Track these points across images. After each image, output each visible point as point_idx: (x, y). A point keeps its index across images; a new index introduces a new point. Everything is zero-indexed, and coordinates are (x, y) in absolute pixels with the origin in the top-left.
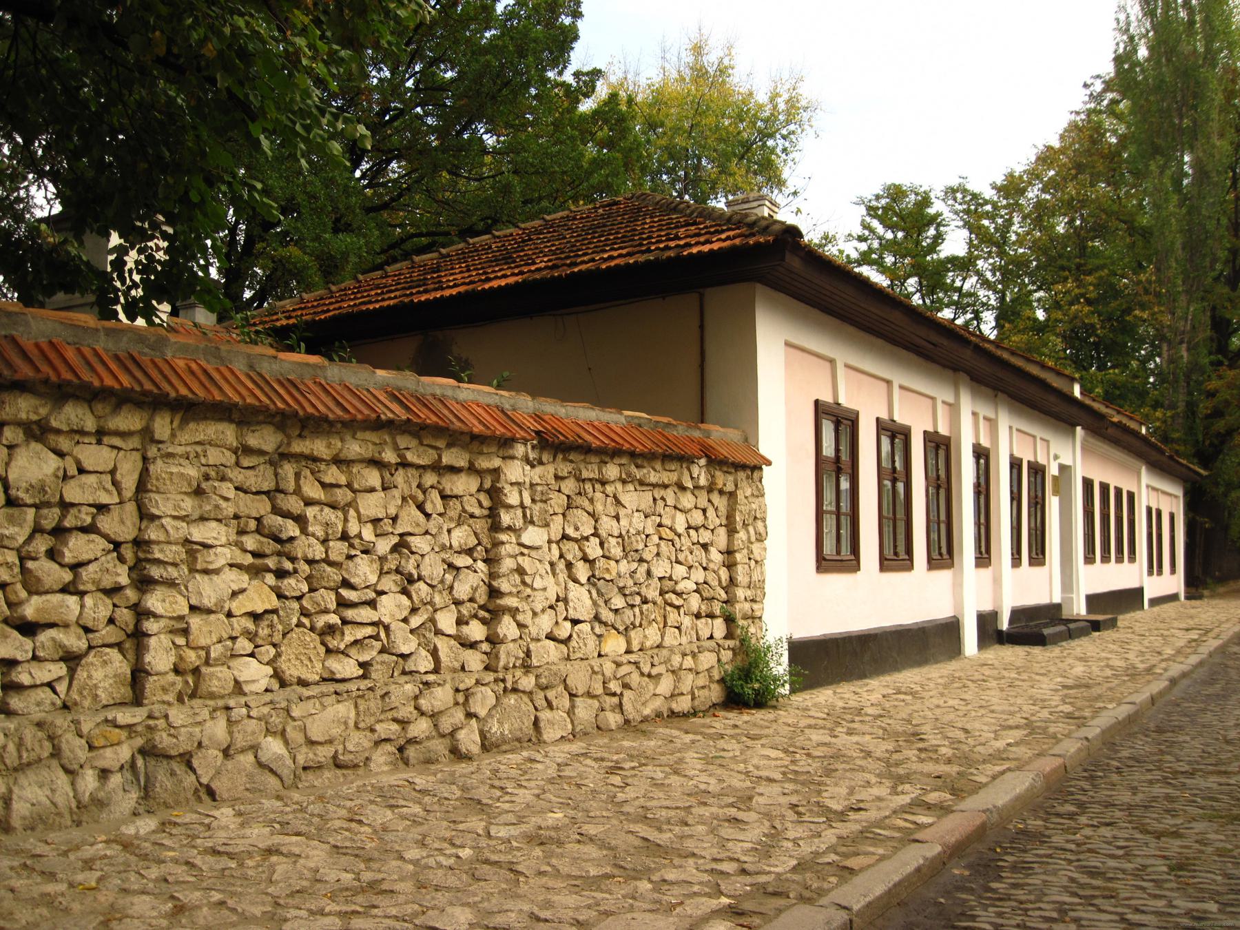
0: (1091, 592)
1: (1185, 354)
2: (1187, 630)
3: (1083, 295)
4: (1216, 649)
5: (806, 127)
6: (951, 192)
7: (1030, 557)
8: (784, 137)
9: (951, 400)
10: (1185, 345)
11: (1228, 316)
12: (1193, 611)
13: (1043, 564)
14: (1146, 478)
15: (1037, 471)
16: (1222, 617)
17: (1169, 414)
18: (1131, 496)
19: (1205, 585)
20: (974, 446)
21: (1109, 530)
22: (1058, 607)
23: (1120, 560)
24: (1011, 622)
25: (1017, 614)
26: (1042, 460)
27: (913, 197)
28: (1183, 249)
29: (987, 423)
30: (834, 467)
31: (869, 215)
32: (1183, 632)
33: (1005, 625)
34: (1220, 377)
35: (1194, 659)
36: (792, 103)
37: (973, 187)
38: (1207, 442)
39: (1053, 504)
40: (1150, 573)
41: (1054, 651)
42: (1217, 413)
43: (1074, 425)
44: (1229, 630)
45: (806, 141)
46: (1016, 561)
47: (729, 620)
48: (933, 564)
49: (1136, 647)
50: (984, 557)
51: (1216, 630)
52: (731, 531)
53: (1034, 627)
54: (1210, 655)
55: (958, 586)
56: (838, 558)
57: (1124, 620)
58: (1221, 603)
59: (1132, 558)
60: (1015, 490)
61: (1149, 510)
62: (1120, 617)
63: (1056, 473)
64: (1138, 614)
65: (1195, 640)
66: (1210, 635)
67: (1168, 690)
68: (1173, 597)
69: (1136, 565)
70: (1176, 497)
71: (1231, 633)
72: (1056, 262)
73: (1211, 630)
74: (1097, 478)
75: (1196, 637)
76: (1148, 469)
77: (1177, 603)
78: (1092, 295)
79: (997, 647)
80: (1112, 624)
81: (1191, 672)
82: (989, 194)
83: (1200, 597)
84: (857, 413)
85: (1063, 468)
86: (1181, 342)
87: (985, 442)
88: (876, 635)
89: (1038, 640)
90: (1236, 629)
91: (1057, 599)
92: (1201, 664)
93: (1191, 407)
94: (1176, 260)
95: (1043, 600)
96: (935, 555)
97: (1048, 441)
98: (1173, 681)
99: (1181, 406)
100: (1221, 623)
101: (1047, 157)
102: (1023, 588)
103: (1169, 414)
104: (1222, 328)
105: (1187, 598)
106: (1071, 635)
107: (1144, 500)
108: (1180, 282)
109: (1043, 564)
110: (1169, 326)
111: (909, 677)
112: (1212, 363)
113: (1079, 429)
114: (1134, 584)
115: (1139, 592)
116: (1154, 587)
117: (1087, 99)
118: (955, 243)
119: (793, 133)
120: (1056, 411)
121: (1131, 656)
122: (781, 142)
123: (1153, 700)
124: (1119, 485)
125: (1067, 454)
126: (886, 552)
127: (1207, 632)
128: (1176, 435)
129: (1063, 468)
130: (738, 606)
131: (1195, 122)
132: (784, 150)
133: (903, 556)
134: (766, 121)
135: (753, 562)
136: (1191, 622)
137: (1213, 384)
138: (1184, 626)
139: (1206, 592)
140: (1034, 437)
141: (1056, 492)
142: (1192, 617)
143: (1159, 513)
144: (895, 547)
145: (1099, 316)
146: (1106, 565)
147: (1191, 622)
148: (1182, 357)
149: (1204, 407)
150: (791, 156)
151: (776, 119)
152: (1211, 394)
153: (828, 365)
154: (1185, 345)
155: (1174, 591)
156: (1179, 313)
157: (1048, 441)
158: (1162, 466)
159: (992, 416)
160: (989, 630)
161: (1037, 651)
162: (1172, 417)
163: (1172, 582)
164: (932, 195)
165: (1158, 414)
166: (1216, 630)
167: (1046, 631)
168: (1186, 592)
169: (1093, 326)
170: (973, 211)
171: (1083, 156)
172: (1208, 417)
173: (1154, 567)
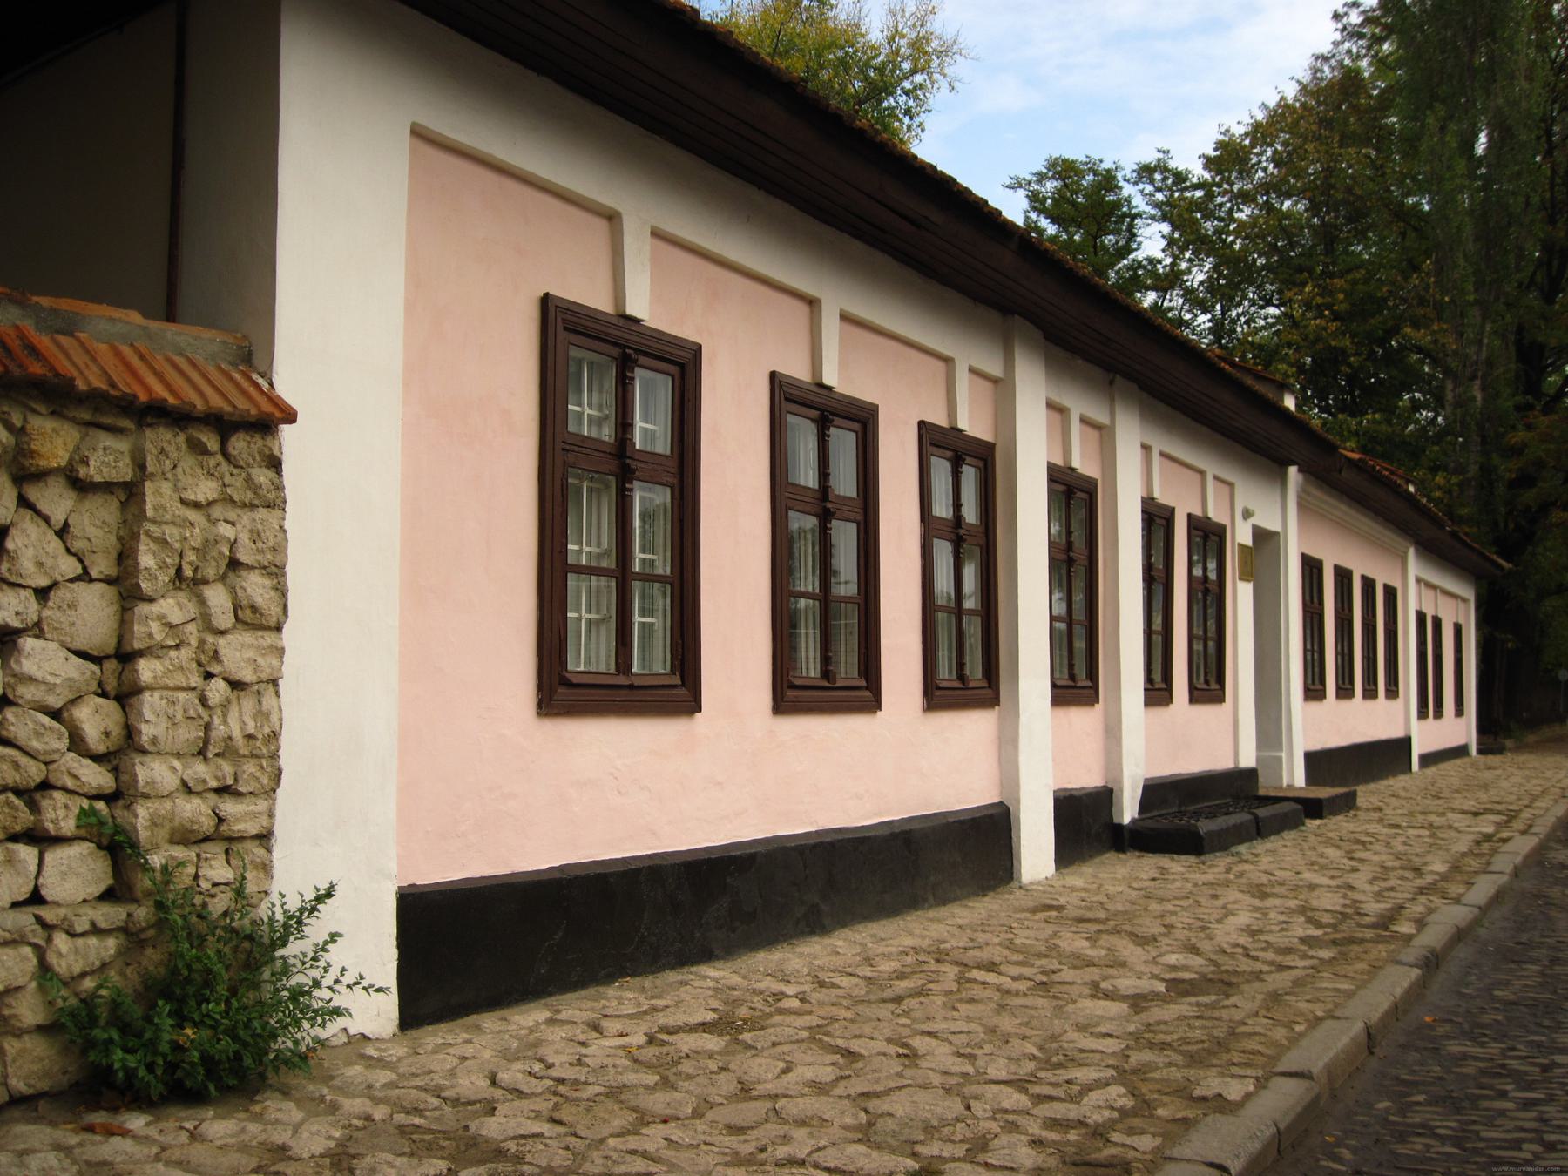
0: (1317, 745)
1: (1479, 396)
2: (1476, 814)
3: (1329, 307)
4: (1527, 857)
5: (936, 76)
6: (1145, 172)
7: (1192, 688)
8: (907, 93)
9: (995, 368)
10: (1478, 382)
11: (1540, 339)
12: (1488, 775)
13: (1219, 699)
14: (1415, 567)
15: (1208, 536)
16: (1535, 786)
17: (1454, 480)
18: (1390, 593)
19: (1508, 733)
20: (1052, 468)
21: (1348, 644)
22: (1251, 774)
23: (1370, 693)
24: (1144, 806)
25: (1155, 792)
26: (1216, 514)
27: (1090, 177)
28: (1477, 239)
29: (1093, 434)
30: (613, 465)
31: (1034, 209)
32: (1468, 819)
33: (1128, 811)
34: (1529, 427)
35: (1483, 889)
36: (918, 45)
37: (1177, 163)
38: (1511, 526)
39: (1241, 599)
40: (1423, 714)
41: (1216, 866)
42: (1525, 480)
43: (1283, 464)
44: (1549, 813)
45: (938, 98)
46: (1158, 692)
47: (119, 849)
48: (936, 697)
49: (1377, 856)
50: (1077, 681)
51: (1526, 814)
52: (127, 590)
53: (1195, 815)
54: (1516, 873)
55: (1007, 743)
56: (622, 680)
57: (1367, 794)
58: (1530, 760)
59: (1392, 693)
60: (1159, 564)
61: (1421, 617)
62: (1361, 790)
63: (1248, 542)
64: (1398, 783)
65: (1488, 838)
66: (1518, 825)
67: (1416, 993)
68: (1460, 751)
69: (1397, 705)
70: (1464, 600)
71: (1551, 819)
72: (1286, 261)
73: (1518, 812)
74: (1332, 555)
75: (1490, 829)
76: (1417, 551)
77: (1466, 760)
78: (1342, 307)
79: (1110, 856)
80: (1347, 803)
81: (1476, 922)
82: (1198, 172)
83: (1500, 751)
84: (697, 351)
85: (1261, 535)
86: (1473, 378)
87: (1084, 463)
88: (752, 858)
89: (1189, 844)
90: (1559, 811)
91: (1248, 760)
92: (1497, 898)
93: (1486, 471)
94: (1465, 256)
95: (1223, 763)
96: (1201, 684)
97: (1231, 485)
98: (1432, 963)
99: (1473, 470)
100: (1534, 798)
101: (1279, 120)
102: (1150, 742)
103: (1454, 480)
104: (1532, 359)
105: (1480, 752)
106: (1261, 830)
107: (1412, 602)
108: (1470, 287)
109: (1219, 699)
110: (1455, 352)
111: (696, 991)
112: (1518, 408)
113: (1293, 471)
114: (1396, 732)
115: (1404, 744)
116: (1427, 737)
117: (1338, 36)
118: (1152, 242)
119: (921, 86)
120: (1260, 442)
121: (1360, 880)
122: (902, 99)
123: (1371, 1038)
124: (1345, 563)
125: (1261, 506)
126: (1057, 675)
127: (1511, 816)
128: (1464, 512)
129: (1261, 535)
130: (142, 811)
131: (1491, 58)
132: (908, 112)
133: (1083, 681)
134: (880, 69)
135: (217, 690)
136: (1483, 797)
137: (1521, 436)
138: (1470, 805)
139: (1509, 743)
140: (1202, 473)
141: (1245, 576)
142: (1485, 787)
143: (1437, 623)
144: (1071, 666)
145: (1352, 337)
146: (1345, 704)
147: (1483, 797)
148: (1474, 399)
149: (1507, 469)
150: (917, 121)
151: (896, 67)
152: (1517, 451)
153: (601, 225)
154: (1478, 382)
155: (1462, 742)
156: (1470, 334)
157: (1231, 485)
158: (1438, 551)
159: (1101, 417)
160: (1084, 822)
161: (1177, 865)
162: (1460, 485)
163: (1456, 729)
164: (1119, 176)
165: (1439, 479)
166: (1526, 814)
167: (1205, 826)
168: (1479, 743)
169: (1343, 351)
170: (1185, 213)
171: (1325, 116)
172: (1512, 485)
173: (1429, 706)
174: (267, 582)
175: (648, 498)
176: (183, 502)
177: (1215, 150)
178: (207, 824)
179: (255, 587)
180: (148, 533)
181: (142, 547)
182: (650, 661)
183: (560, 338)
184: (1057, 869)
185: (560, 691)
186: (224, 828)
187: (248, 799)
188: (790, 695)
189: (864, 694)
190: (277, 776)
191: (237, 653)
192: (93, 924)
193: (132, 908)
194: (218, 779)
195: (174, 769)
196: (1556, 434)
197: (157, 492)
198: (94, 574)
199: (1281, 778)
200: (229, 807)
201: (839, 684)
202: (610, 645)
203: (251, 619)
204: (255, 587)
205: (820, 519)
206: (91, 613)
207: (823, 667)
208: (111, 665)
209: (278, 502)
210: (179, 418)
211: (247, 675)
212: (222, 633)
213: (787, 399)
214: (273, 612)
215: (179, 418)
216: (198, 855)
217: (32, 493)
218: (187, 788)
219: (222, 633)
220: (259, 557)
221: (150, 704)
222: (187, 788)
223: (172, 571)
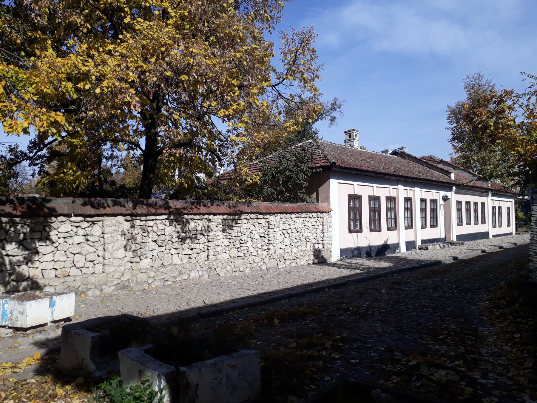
7: (431, 225)
13: (436, 226)
68: (511, 234)
109: (436, 226)
133: (435, 224)
175: (358, 213)
182: (393, 226)
185: (350, 231)
188: (371, 230)
189: (380, 230)
196: (23, 53)
202: (355, 227)
204: (330, 224)
205: (375, 211)
206: (321, 227)
207: (375, 227)
215: (326, 212)
217: (59, 230)
221: (325, 234)
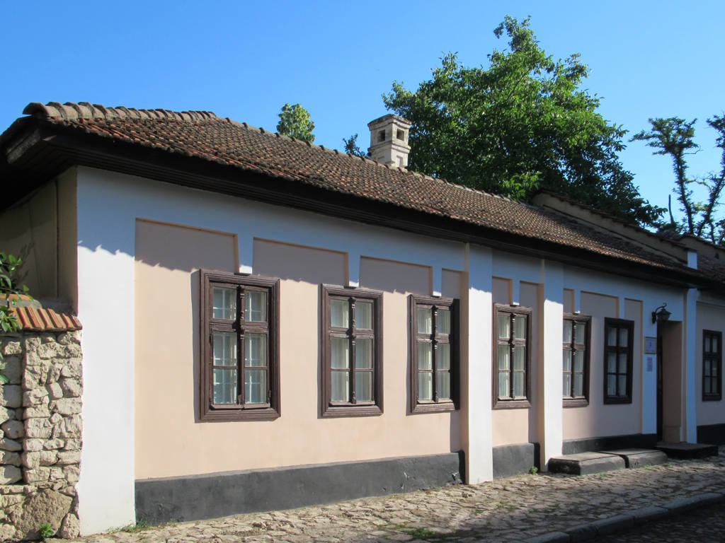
109: (627, 399)
174: (75, 381)
176: (42, 359)
177: (24, 113)
178: (53, 460)
179: (71, 384)
180: (27, 369)
181: (26, 373)
183: (207, 287)
184: (495, 475)
185: (205, 410)
186: (60, 461)
187: (69, 452)
190: (81, 444)
191: (64, 405)
192: (10, 491)
193: (26, 486)
194: (57, 445)
195: (41, 443)
197: (31, 356)
198: (11, 382)
199: (679, 437)
200: (62, 455)
201: (357, 404)
203: (68, 393)
208: (19, 411)
209: (79, 355)
210: (37, 333)
211: (68, 412)
212: (58, 399)
213: (330, 294)
214: (326, 414)
215: (37, 333)
216: (51, 470)
218: (45, 449)
219: (58, 399)
220: (72, 374)
222: (45, 449)
223: (38, 381)
